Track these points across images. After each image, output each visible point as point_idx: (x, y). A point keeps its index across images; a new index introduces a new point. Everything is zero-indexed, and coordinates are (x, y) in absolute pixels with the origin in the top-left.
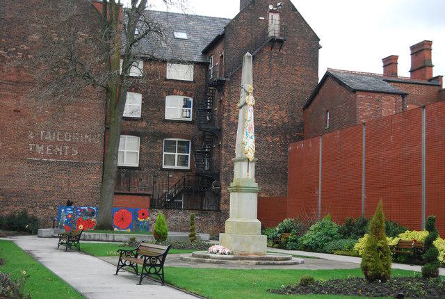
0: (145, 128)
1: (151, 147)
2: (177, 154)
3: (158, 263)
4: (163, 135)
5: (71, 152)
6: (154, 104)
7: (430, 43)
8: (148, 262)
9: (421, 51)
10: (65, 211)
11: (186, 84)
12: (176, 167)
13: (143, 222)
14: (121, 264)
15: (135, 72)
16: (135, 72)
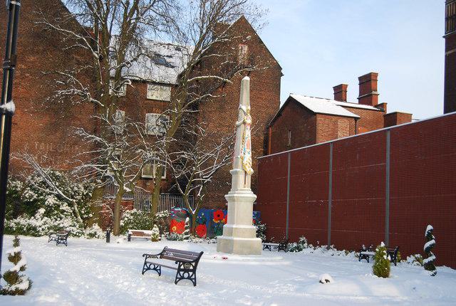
3: (191, 268)
7: (376, 75)
8: (182, 267)
9: (368, 83)
14: (179, 276)
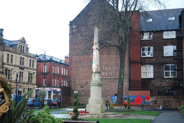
0: (155, 61)
1: (158, 69)
2: (170, 71)
4: (162, 64)
5: (115, 74)
6: (159, 50)
10: (115, 98)
11: (170, 40)
12: (170, 77)
13: (148, 102)
15: (146, 37)
16: (146, 37)
